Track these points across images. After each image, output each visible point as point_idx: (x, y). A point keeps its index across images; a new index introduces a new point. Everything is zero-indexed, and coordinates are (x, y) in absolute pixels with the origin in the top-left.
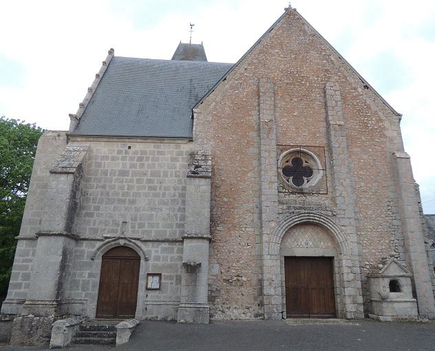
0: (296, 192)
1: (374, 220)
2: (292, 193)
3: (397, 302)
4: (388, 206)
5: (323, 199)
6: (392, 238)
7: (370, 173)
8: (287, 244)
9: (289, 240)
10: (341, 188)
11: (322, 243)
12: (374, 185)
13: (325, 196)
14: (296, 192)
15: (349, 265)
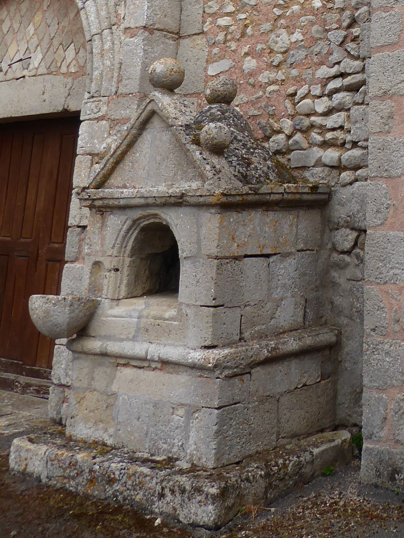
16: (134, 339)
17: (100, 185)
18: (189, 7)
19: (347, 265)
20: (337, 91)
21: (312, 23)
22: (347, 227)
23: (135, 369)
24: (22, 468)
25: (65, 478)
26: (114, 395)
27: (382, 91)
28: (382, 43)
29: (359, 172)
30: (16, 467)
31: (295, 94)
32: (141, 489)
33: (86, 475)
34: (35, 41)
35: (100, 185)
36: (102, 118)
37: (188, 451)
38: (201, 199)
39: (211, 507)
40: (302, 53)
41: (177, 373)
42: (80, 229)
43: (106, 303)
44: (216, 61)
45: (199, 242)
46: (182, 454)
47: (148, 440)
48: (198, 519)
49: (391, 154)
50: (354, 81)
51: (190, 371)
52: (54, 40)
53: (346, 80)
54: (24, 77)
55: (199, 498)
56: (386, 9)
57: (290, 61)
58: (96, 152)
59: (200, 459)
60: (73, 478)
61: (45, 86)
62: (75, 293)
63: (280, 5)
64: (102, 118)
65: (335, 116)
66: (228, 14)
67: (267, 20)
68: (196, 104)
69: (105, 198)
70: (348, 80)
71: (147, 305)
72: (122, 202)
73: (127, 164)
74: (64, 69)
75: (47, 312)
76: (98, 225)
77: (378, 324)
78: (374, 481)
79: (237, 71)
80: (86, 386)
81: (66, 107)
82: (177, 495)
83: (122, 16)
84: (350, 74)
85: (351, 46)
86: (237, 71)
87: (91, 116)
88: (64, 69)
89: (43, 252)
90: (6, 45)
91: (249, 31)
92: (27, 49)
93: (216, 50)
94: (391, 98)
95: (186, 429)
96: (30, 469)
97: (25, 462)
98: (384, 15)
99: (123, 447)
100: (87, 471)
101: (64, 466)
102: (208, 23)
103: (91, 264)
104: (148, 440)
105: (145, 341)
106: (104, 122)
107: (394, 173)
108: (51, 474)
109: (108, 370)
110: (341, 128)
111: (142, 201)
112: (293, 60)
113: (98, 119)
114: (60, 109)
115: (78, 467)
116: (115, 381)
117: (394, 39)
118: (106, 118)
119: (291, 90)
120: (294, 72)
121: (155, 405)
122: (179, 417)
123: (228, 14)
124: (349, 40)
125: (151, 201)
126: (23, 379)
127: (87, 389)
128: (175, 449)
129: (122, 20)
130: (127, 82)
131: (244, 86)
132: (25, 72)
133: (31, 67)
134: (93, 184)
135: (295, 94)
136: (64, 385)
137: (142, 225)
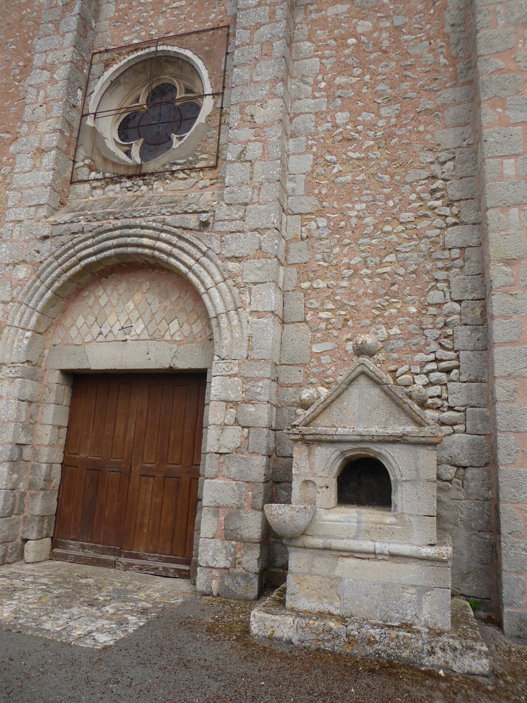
0: (121, 176)
1: (370, 236)
2: (113, 181)
3: (351, 553)
4: (434, 177)
5: (201, 184)
6: (436, 296)
7: (374, 74)
8: (73, 332)
9: (80, 321)
10: (246, 133)
11: (174, 326)
12: (383, 112)
13: (210, 174)
14: (121, 176)
15: (232, 397)
16: (355, 538)
17: (307, 425)
18: (291, 302)
19: (450, 489)
20: (433, 371)
21: (409, 323)
22: (448, 464)
23: (359, 560)
24: (269, 633)
25: (319, 640)
26: (340, 579)
27: (507, 373)
28: (505, 339)
29: (455, 427)
30: (260, 633)
31: (395, 371)
32: (406, 648)
33: (344, 638)
34: (136, 314)
35: (307, 425)
36: (235, 375)
37: (423, 619)
38: (423, 439)
39: (485, 661)
40: (401, 343)
41: (406, 563)
42: (218, 455)
43: (321, 511)
44: (318, 343)
45: (417, 470)
46: (416, 621)
47: (378, 610)
48: (473, 670)
49: (518, 417)
50: (449, 365)
51: (421, 562)
52: (156, 315)
53: (441, 364)
54: (126, 340)
55: (472, 654)
56: (505, 317)
57: (390, 347)
58: (231, 400)
59: (435, 624)
60: (329, 641)
61: (148, 349)
62: (218, 501)
63: (378, 307)
64: (235, 375)
65: (433, 388)
66: (328, 310)
67: (367, 318)
68: (302, 372)
69: (318, 434)
70: (443, 365)
71: (360, 514)
72: (336, 438)
73: (335, 409)
74: (168, 337)
75: (292, 517)
76: (305, 454)
77: (514, 530)
78: (517, 633)
79: (340, 351)
80: (306, 571)
81: (172, 365)
82: (449, 652)
83: (248, 302)
84: (444, 361)
85: (446, 342)
86: (340, 351)
87: (224, 373)
88: (168, 337)
89: (136, 469)
90: (105, 315)
91: (350, 323)
92: (129, 319)
93: (319, 335)
94: (514, 378)
95: (419, 603)
96: (278, 634)
97: (272, 630)
98: (505, 321)
99: (352, 616)
100: (344, 635)
101: (317, 632)
102: (309, 315)
103: (301, 482)
104: (378, 610)
105: (368, 540)
106: (237, 379)
107: (521, 429)
108: (302, 638)
109: (330, 560)
110: (439, 397)
111: (358, 438)
112: (393, 347)
113: (230, 376)
114: (167, 366)
115: (332, 633)
116: (337, 568)
117: (516, 338)
118: (238, 375)
119: (393, 368)
120: (395, 355)
121: (384, 586)
122: (410, 594)
123: (328, 310)
124: (442, 337)
125: (367, 438)
126: (124, 560)
127: (307, 574)
128: (409, 617)
129: (248, 305)
130: (258, 350)
131: (348, 362)
132: (127, 337)
133: (133, 333)
134: (303, 423)
135: (395, 371)
136: (212, 567)
137: (348, 455)
